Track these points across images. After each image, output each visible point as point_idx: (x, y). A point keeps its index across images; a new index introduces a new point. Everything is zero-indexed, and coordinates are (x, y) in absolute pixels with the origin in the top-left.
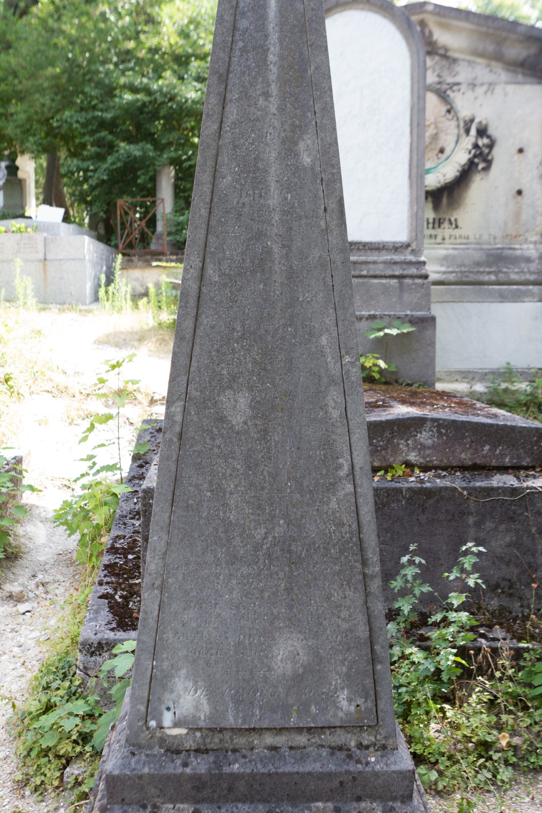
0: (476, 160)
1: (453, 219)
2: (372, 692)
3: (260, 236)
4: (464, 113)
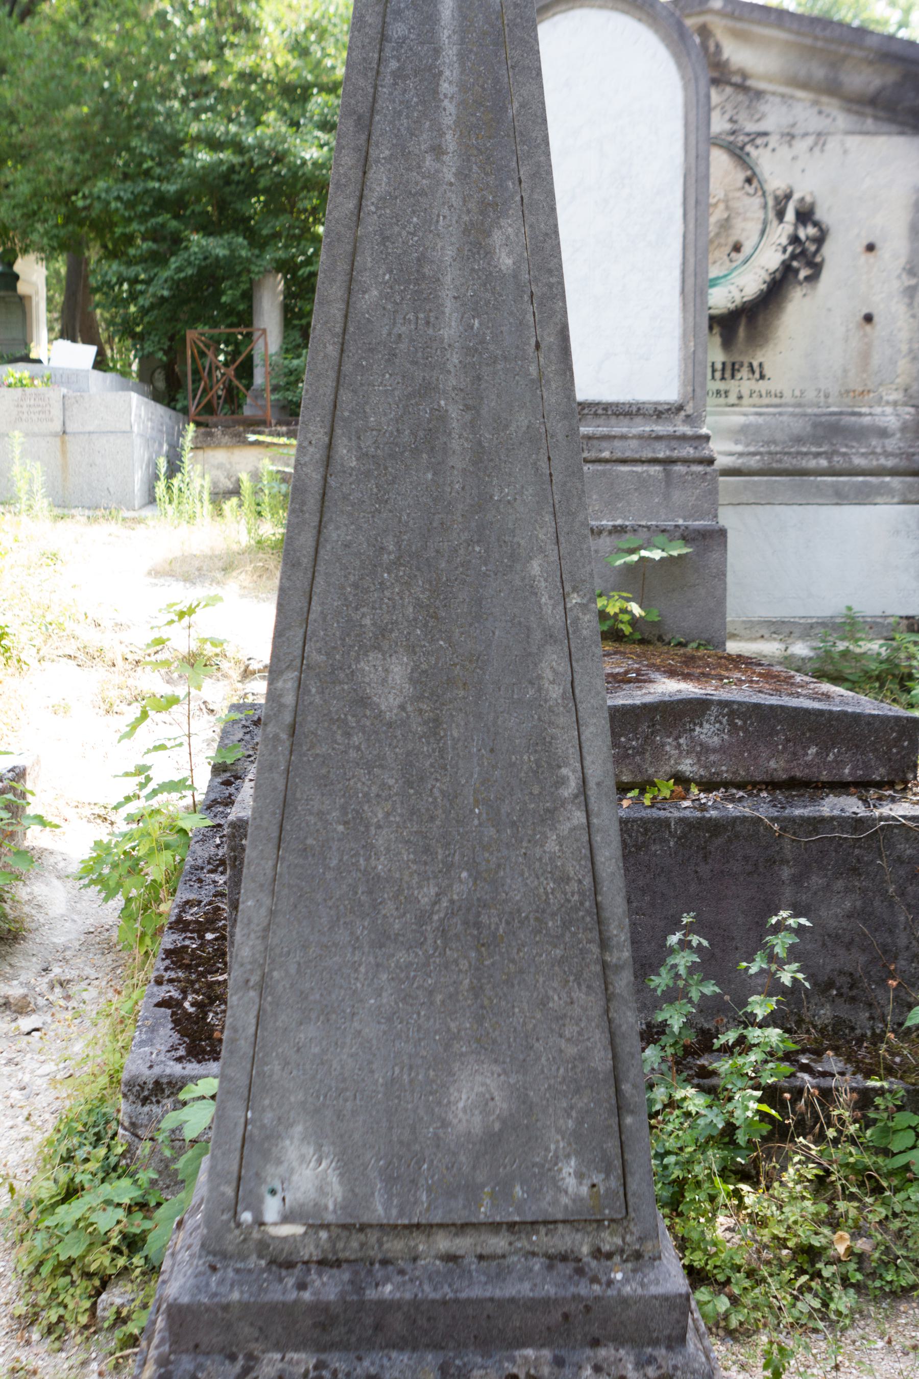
0: (795, 264)
1: (755, 364)
2: (617, 1163)
3: (427, 390)
4: (776, 183)
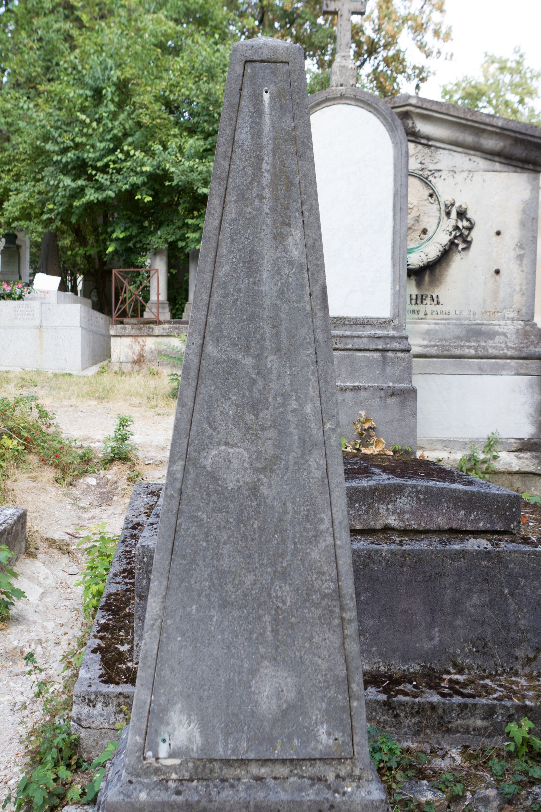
0: (456, 241)
1: (434, 296)
2: (349, 727)
3: (252, 317)
4: (445, 197)
